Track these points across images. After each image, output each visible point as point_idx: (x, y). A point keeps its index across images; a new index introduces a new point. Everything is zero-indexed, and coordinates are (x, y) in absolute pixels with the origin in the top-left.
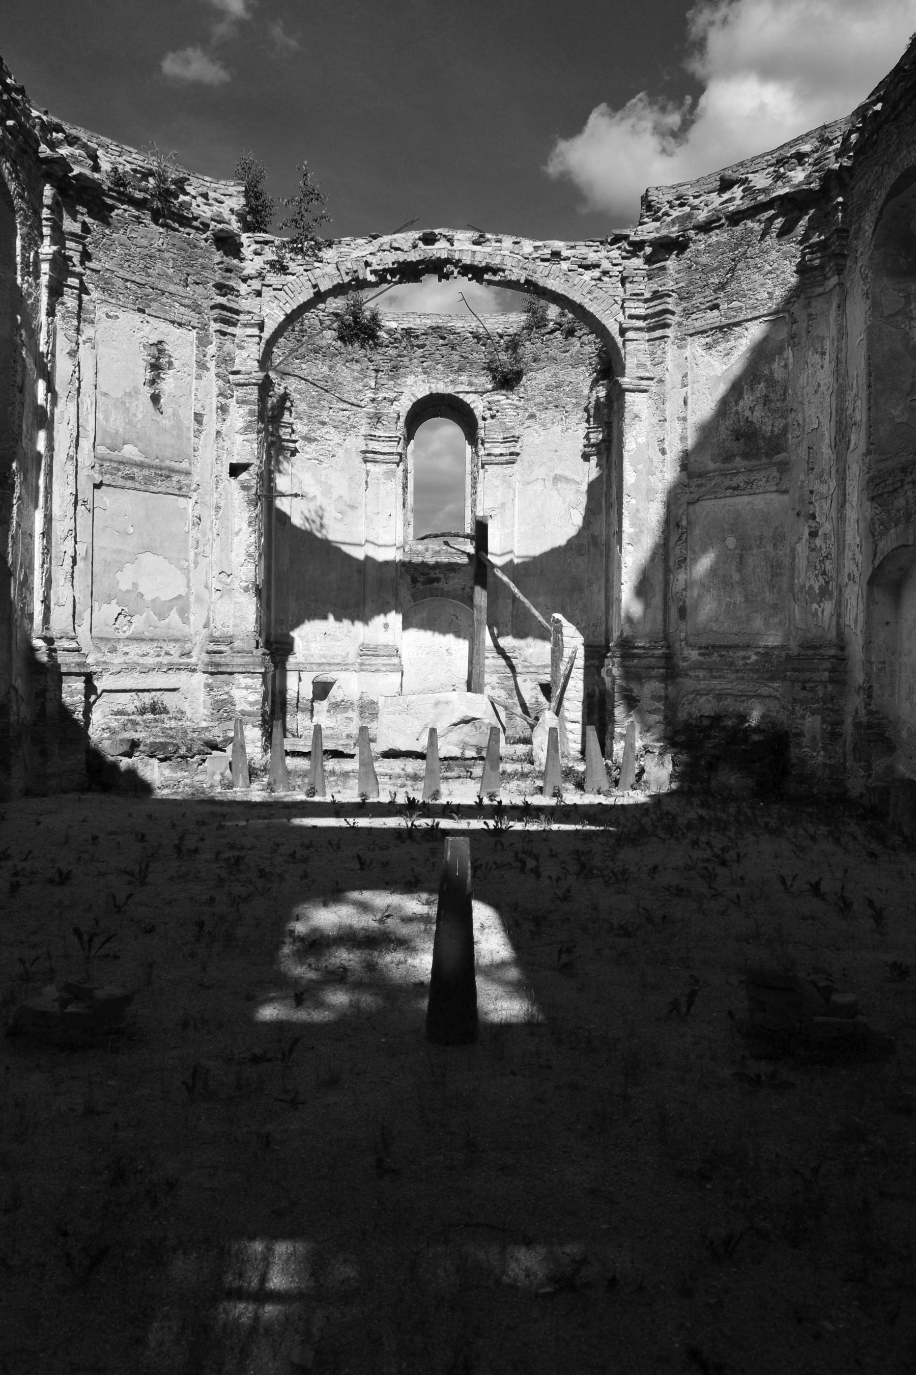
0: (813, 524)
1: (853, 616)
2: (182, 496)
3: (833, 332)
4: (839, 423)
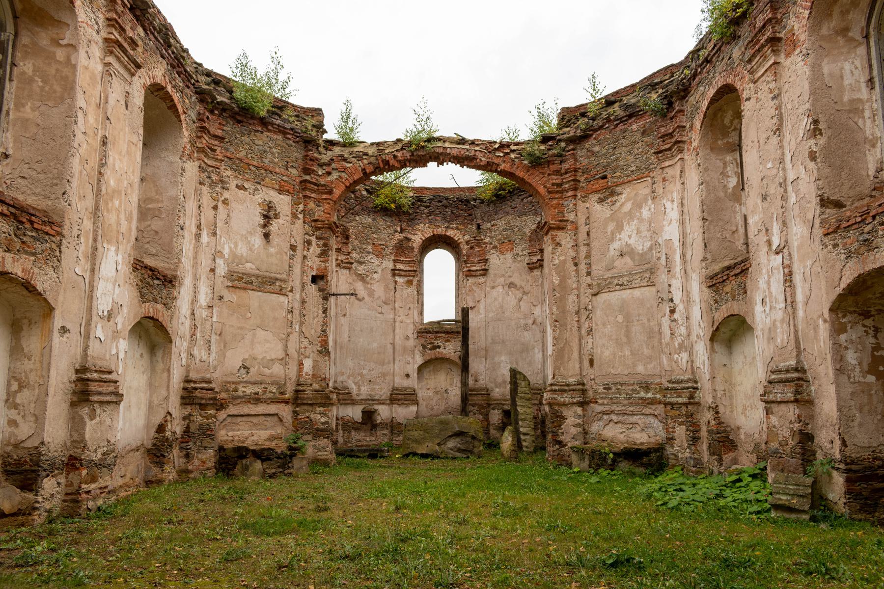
0: (672, 305)
1: (701, 362)
2: (282, 294)
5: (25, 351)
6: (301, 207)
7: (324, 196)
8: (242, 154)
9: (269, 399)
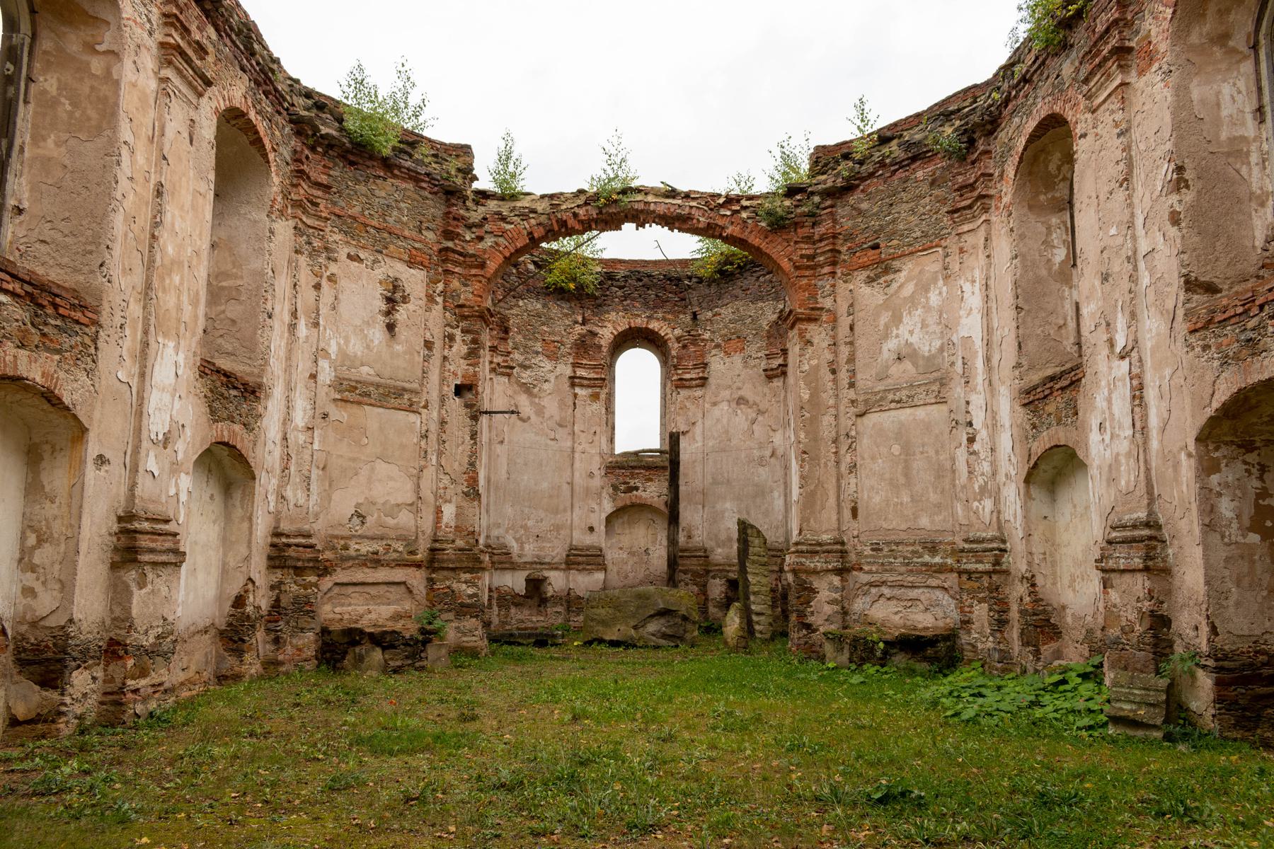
0: (970, 430)
6: (440, 286)
9: (393, 560)
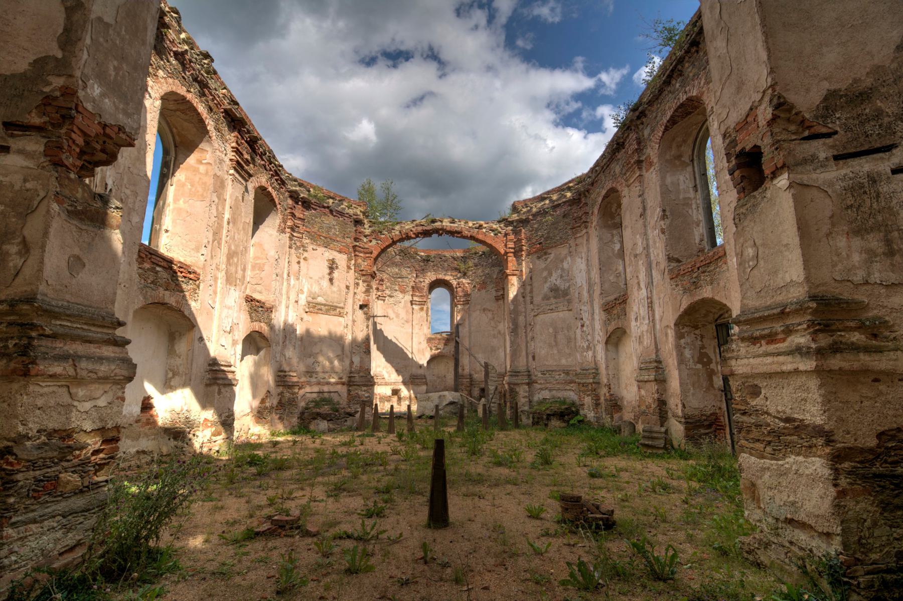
3: (585, 249)
4: (589, 283)
5: (177, 352)
7: (367, 255)
8: (315, 230)
